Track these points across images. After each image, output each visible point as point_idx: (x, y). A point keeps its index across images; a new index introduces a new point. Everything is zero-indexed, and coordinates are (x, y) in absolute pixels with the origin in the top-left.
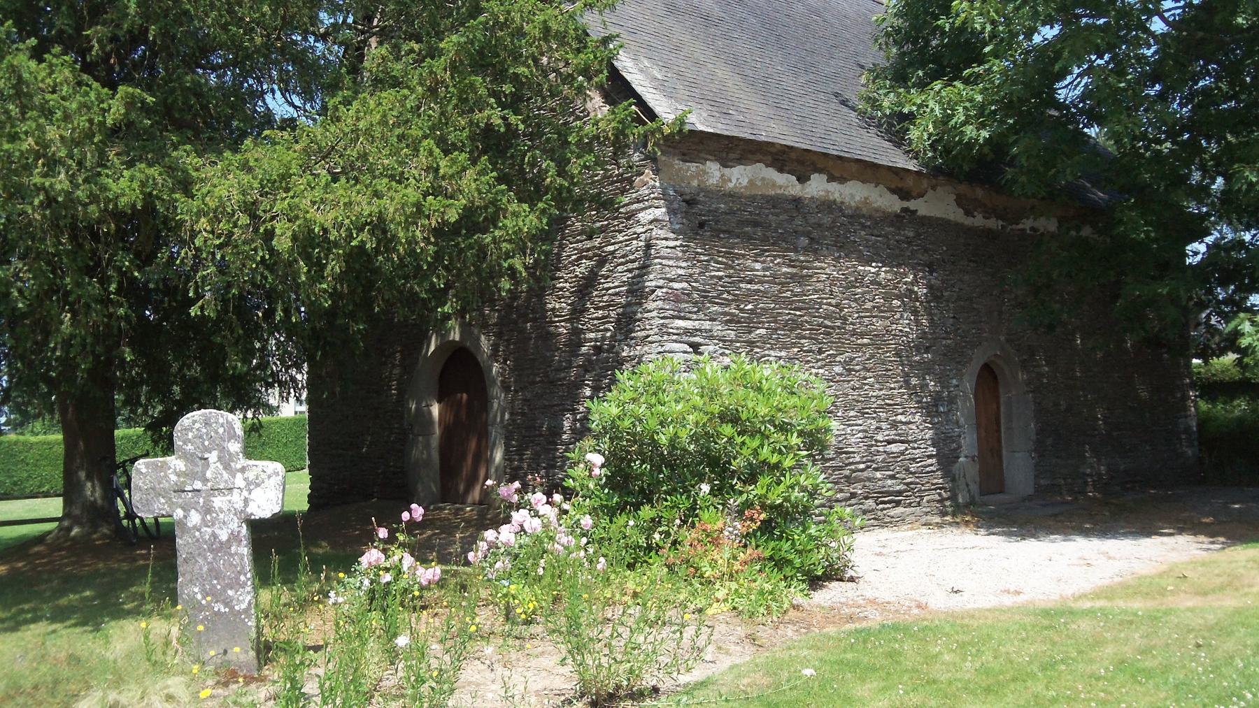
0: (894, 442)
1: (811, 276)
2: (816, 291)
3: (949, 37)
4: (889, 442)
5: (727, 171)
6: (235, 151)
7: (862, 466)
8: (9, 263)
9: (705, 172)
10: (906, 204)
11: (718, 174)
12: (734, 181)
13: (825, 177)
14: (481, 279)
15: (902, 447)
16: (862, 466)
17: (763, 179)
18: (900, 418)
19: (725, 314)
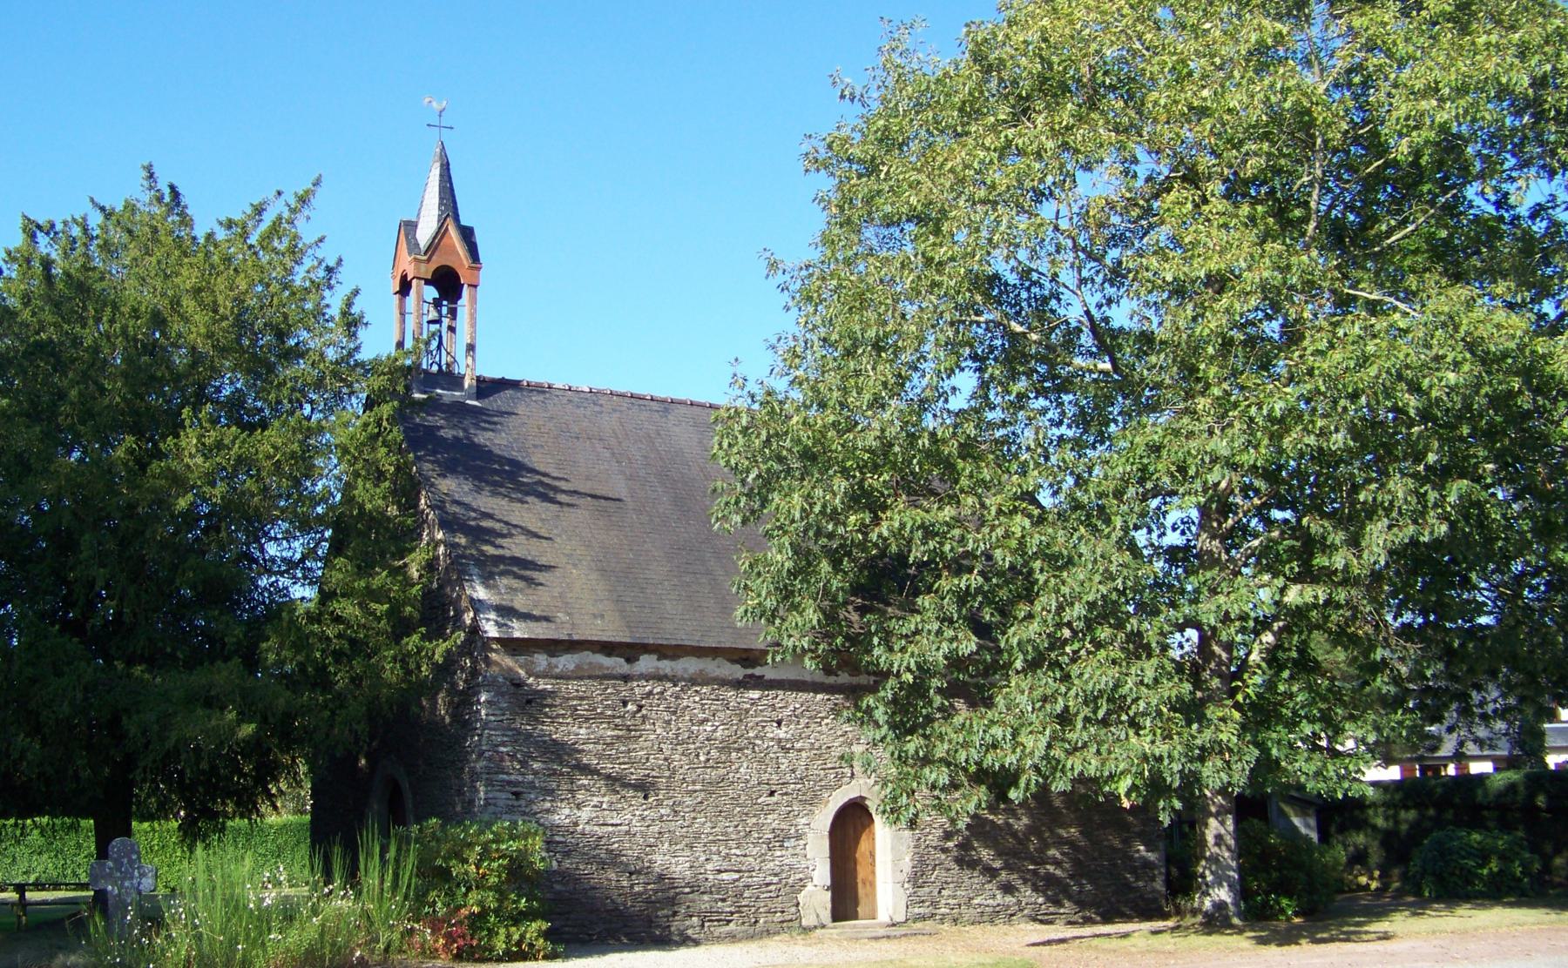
0: (726, 871)
1: (640, 736)
2: (642, 749)
3: (449, 618)
4: (720, 872)
5: (554, 660)
6: (1501, 238)
7: (687, 890)
8: (946, 657)
9: (533, 663)
10: (749, 671)
11: (545, 663)
12: (561, 667)
13: (655, 657)
14: (1463, 697)
15: (736, 876)
16: (687, 890)
17: (590, 663)
18: (733, 851)
19: (548, 769)
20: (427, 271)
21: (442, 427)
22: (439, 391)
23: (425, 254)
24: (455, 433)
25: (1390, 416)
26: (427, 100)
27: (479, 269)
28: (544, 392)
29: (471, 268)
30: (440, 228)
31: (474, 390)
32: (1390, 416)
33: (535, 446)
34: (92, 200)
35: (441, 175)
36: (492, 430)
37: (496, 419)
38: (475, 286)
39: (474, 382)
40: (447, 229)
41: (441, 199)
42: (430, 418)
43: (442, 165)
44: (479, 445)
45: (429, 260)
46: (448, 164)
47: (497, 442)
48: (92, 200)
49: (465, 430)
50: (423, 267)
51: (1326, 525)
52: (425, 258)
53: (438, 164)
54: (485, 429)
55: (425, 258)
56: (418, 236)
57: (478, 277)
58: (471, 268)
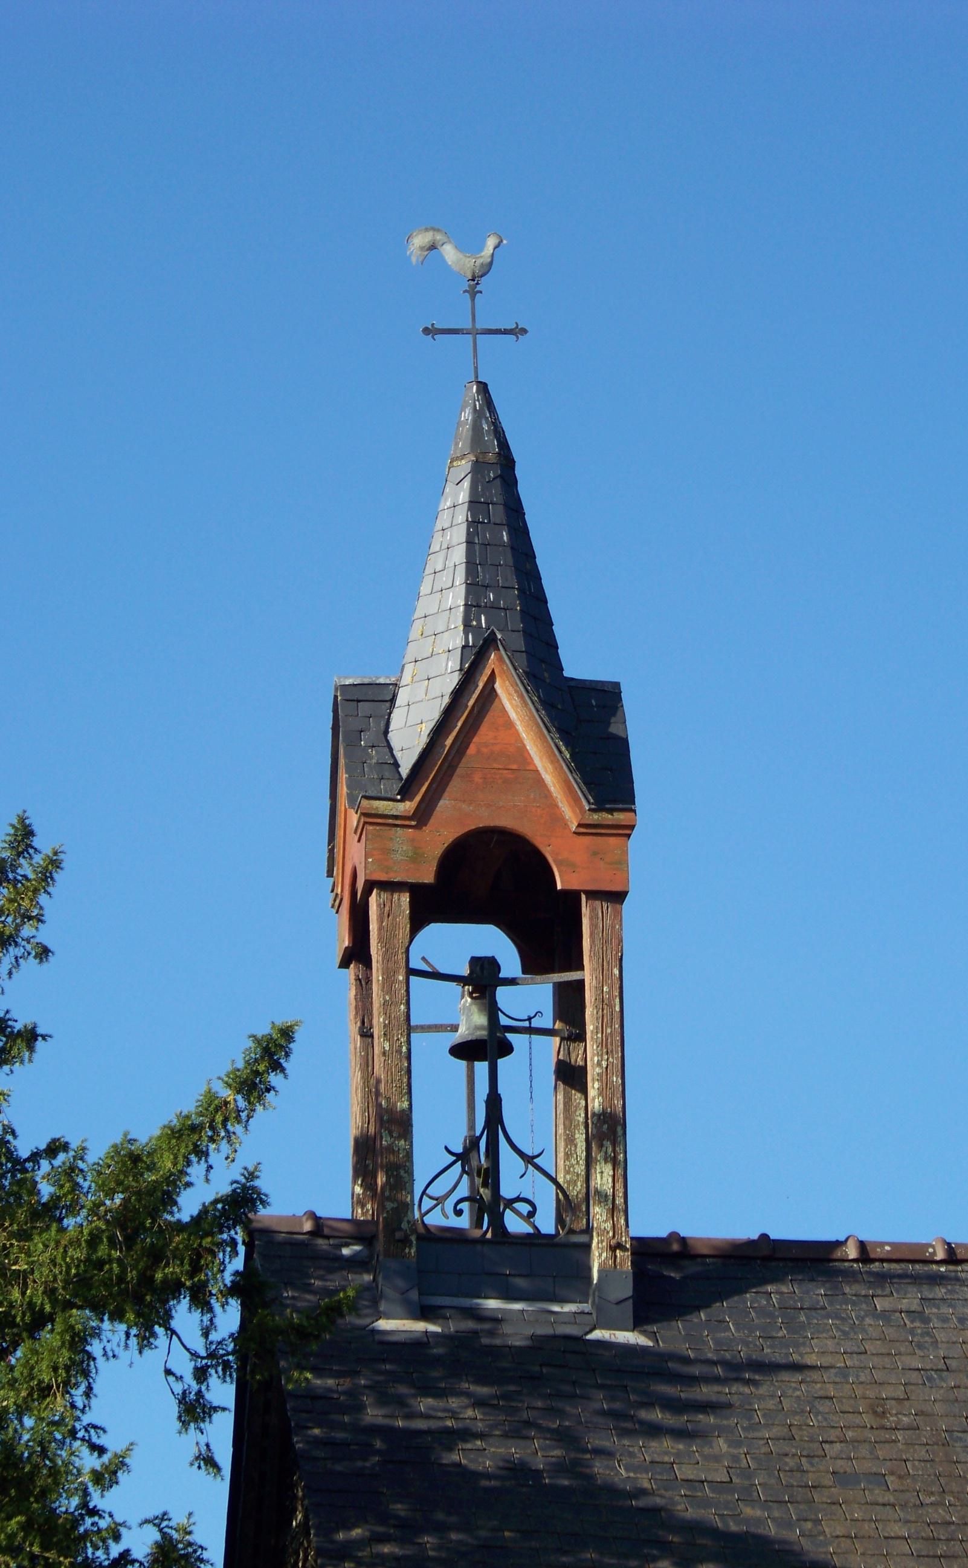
20: (416, 857)
21: (466, 1434)
22: (492, 1304)
23: (406, 790)
24: (515, 1451)
25: (49, 1480)
26: (420, 240)
27: (626, 830)
28: (936, 1280)
29: (587, 829)
30: (458, 695)
31: (626, 1289)
32: (49, 1480)
33: (842, 1479)
34: (446, 1148)
35: (474, 503)
36: (680, 1434)
37: (706, 1392)
38: (617, 897)
39: (625, 1260)
40: (489, 695)
41: (474, 587)
42: (424, 1404)
43: (478, 468)
44: (612, 1491)
45: (422, 817)
46: (506, 461)
47: (684, 1472)
48: (446, 1148)
49: (565, 1437)
50: (401, 840)
51: (607, 1354)
52: (408, 807)
53: (465, 466)
54: (654, 1431)
55: (408, 807)
56: (394, 738)
57: (621, 863)
58: (587, 829)
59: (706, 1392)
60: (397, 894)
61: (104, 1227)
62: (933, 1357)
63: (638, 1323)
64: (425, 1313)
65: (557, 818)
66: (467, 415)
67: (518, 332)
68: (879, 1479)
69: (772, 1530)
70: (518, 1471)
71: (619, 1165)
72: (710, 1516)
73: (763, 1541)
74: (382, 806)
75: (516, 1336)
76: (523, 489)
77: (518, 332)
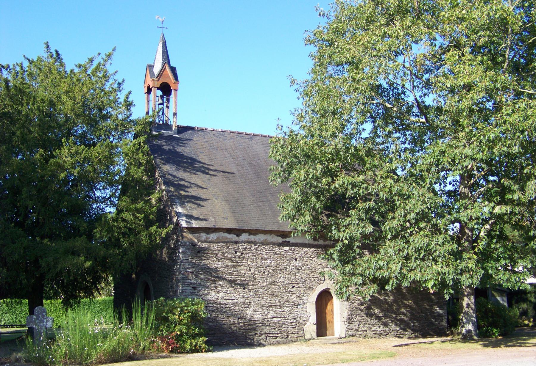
20: (158, 84)
23: (157, 77)
26: (157, 17)
27: (178, 83)
29: (175, 83)
33: (200, 152)
34: (24, 56)
37: (185, 142)
38: (177, 90)
39: (177, 128)
40: (165, 68)
43: (163, 43)
44: (179, 152)
45: (158, 80)
46: (165, 42)
47: (185, 151)
48: (24, 56)
49: (173, 146)
50: (156, 83)
52: (157, 79)
53: (162, 42)
54: (181, 146)
55: (157, 79)
56: (154, 71)
57: (178, 87)
58: (175, 83)
59: (185, 142)
60: (500, 206)
61: (519, 320)
62: (206, 140)
63: (178, 134)
64: (157, 132)
65: (171, 82)
66: (161, 37)
67: (167, 28)
68: (203, 153)
69: (195, 157)
70: (169, 149)
71: (176, 118)
72: (189, 156)
73: (194, 158)
74: (154, 79)
75: (165, 135)
76: (167, 45)
77: (167, 28)
